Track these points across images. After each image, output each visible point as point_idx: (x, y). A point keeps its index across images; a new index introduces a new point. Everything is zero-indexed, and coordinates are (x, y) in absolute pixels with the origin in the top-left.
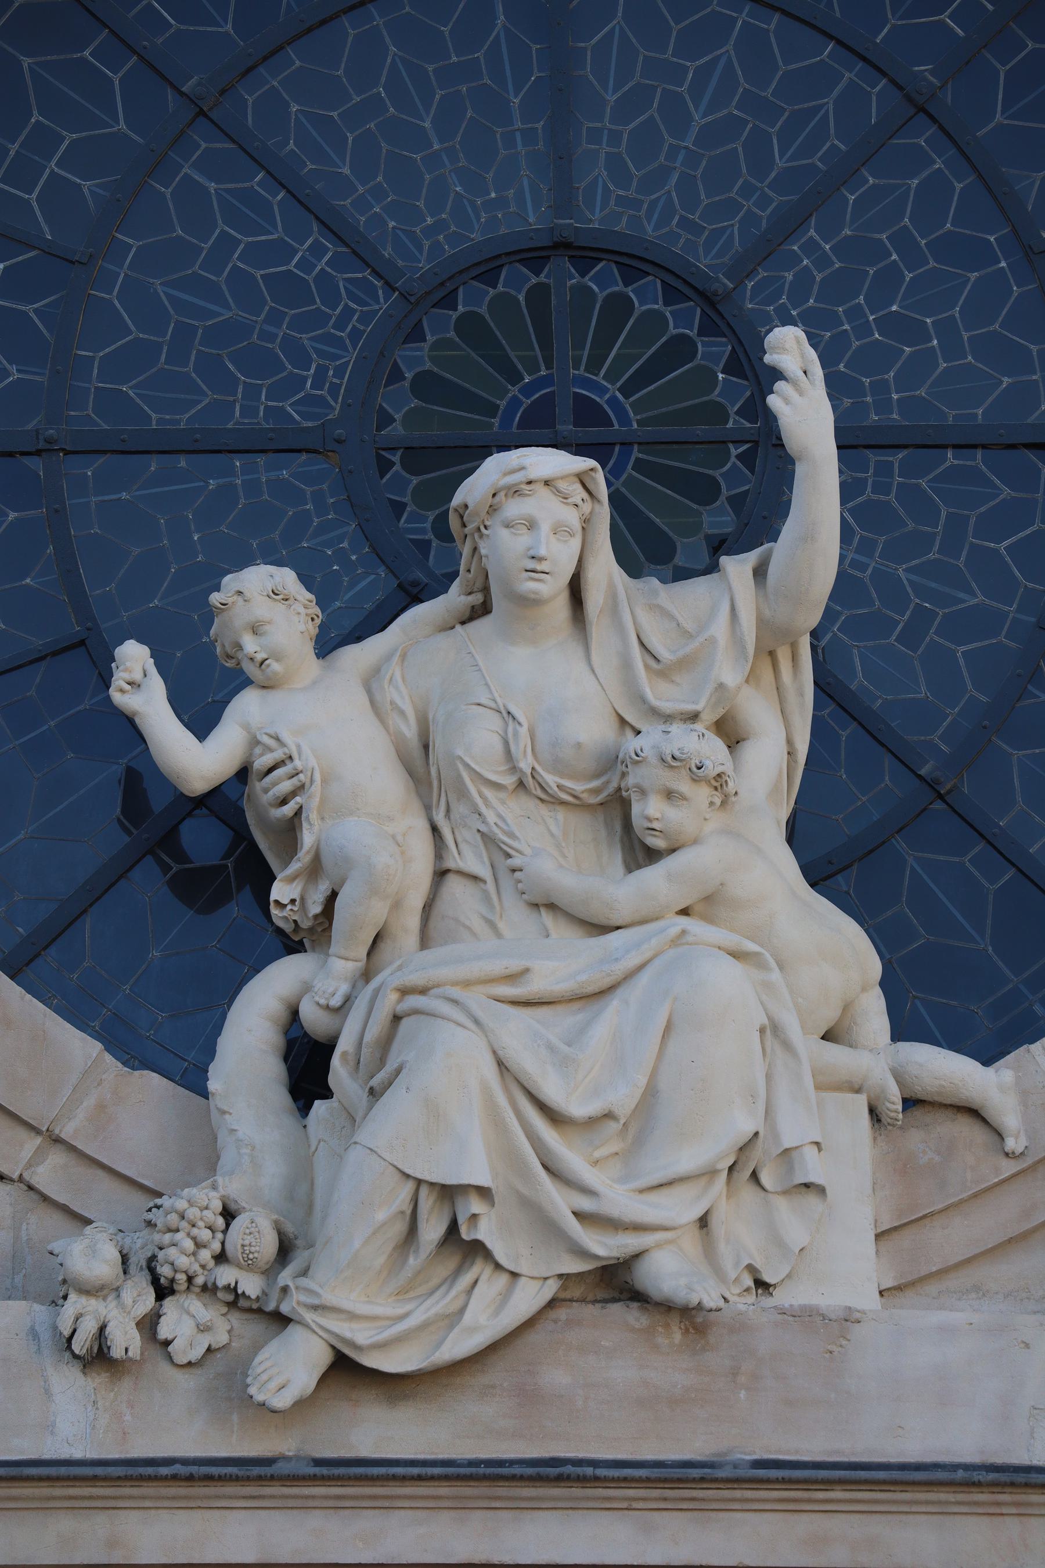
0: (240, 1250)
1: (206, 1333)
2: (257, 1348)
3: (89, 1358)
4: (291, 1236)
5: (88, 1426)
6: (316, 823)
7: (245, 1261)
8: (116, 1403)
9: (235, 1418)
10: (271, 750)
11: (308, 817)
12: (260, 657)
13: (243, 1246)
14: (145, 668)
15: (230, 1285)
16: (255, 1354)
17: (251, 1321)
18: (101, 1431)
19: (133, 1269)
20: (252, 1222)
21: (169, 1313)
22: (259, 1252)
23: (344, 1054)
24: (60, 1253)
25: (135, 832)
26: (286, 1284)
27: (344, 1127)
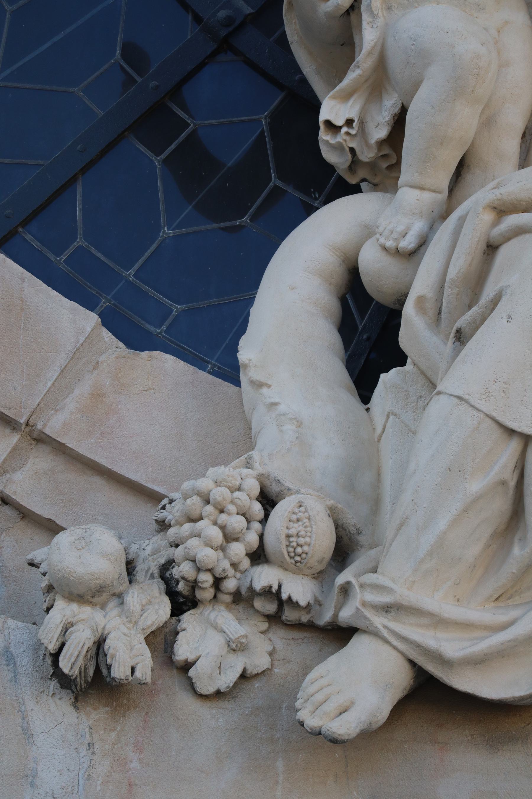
0: (284, 542)
1: (239, 654)
2: (306, 670)
3: (82, 682)
4: (353, 530)
5: (80, 774)
6: (380, 14)
7: (291, 558)
8: (119, 746)
9: (280, 764)
13: (288, 536)
15: (271, 587)
16: (305, 675)
17: (300, 641)
18: (99, 782)
19: (140, 575)
20: (300, 506)
21: (190, 629)
22: (309, 545)
23: (421, 300)
24: (43, 561)
25: (139, 80)
26: (346, 580)
27: (421, 397)
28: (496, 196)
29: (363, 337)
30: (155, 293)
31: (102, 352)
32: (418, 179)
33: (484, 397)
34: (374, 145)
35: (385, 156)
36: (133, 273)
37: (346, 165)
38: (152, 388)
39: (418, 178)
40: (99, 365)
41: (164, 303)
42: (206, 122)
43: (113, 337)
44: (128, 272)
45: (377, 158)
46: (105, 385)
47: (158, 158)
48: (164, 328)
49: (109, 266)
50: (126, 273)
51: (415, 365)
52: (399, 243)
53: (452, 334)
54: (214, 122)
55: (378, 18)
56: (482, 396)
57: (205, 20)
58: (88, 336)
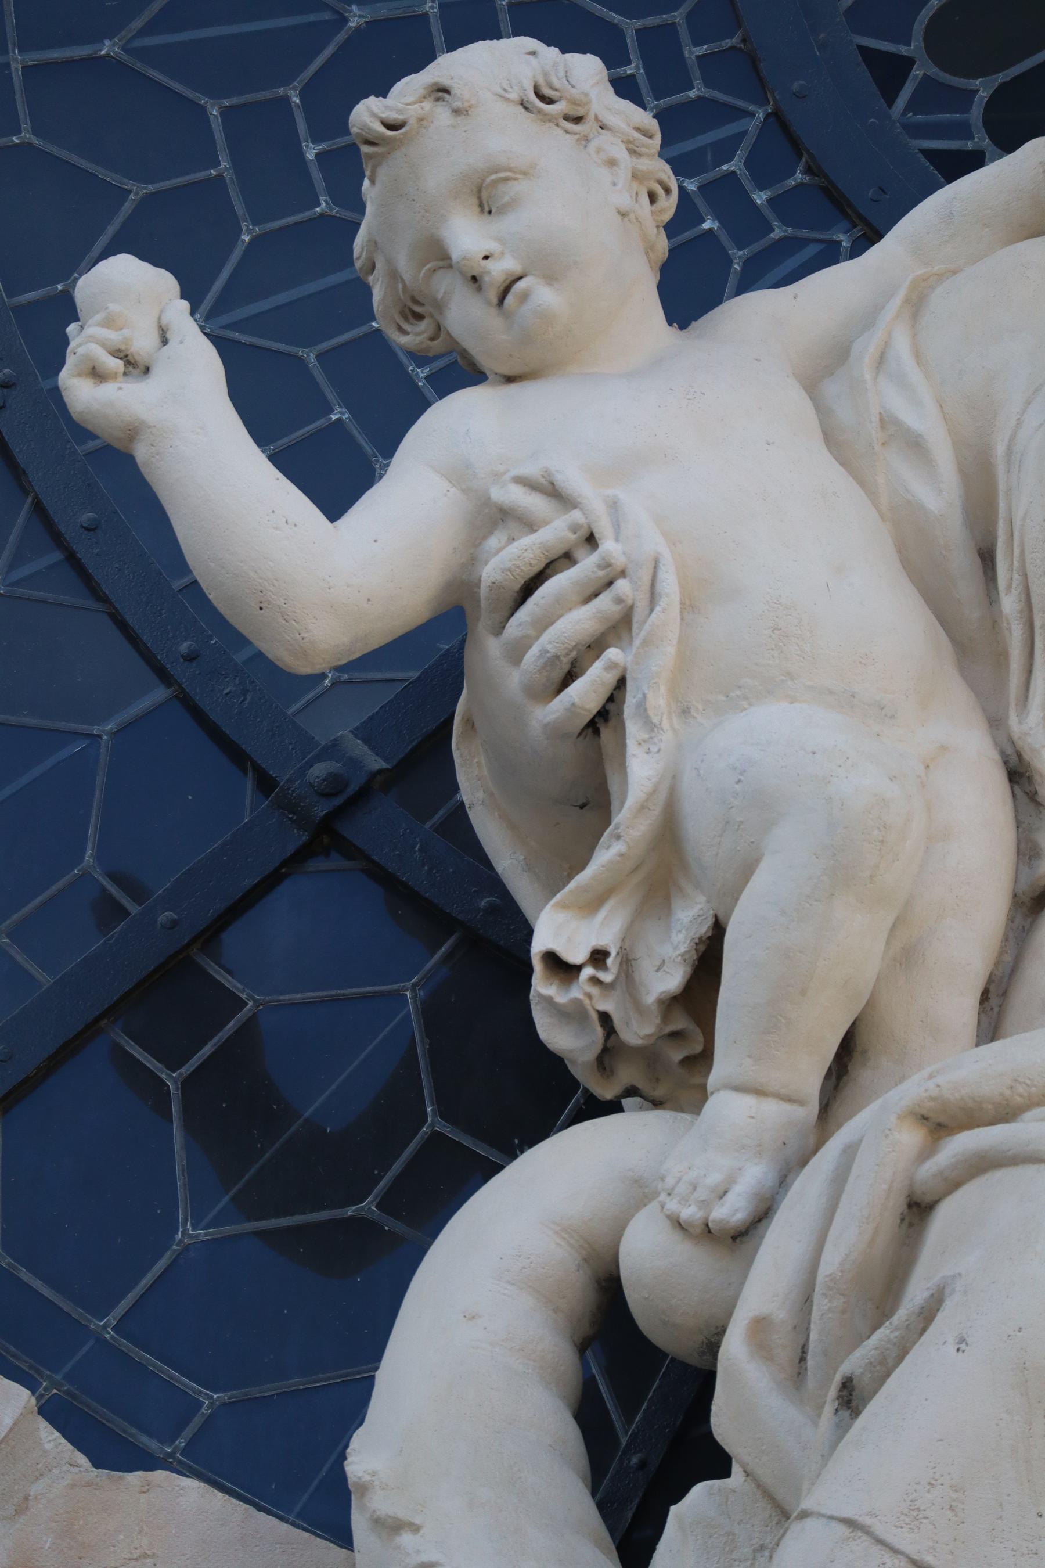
6: (665, 724)
10: (530, 525)
11: (642, 707)
12: (499, 269)
14: (164, 323)
23: (760, 1326)
25: (134, 909)
28: (926, 1091)
29: (629, 1462)
30: (161, 1367)
31: (37, 1474)
32: (752, 1071)
33: (907, 1520)
34: (654, 1008)
35: (676, 1036)
36: (114, 1323)
37: (590, 1055)
38: (149, 1553)
39: (753, 1068)
40: (31, 1503)
41: (183, 1388)
42: (282, 998)
43: (63, 1441)
44: (101, 1321)
45: (660, 1037)
46: (42, 1548)
47: (174, 1075)
48: (181, 1442)
49: (60, 1308)
50: (96, 1324)
51: (748, 1475)
52: (711, 1212)
53: (833, 1392)
54: (299, 997)
55: (662, 732)
56: (903, 1517)
57: (282, 783)
58: (5, 1437)
